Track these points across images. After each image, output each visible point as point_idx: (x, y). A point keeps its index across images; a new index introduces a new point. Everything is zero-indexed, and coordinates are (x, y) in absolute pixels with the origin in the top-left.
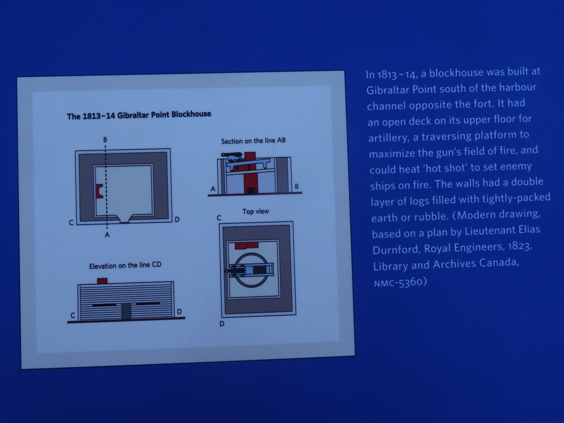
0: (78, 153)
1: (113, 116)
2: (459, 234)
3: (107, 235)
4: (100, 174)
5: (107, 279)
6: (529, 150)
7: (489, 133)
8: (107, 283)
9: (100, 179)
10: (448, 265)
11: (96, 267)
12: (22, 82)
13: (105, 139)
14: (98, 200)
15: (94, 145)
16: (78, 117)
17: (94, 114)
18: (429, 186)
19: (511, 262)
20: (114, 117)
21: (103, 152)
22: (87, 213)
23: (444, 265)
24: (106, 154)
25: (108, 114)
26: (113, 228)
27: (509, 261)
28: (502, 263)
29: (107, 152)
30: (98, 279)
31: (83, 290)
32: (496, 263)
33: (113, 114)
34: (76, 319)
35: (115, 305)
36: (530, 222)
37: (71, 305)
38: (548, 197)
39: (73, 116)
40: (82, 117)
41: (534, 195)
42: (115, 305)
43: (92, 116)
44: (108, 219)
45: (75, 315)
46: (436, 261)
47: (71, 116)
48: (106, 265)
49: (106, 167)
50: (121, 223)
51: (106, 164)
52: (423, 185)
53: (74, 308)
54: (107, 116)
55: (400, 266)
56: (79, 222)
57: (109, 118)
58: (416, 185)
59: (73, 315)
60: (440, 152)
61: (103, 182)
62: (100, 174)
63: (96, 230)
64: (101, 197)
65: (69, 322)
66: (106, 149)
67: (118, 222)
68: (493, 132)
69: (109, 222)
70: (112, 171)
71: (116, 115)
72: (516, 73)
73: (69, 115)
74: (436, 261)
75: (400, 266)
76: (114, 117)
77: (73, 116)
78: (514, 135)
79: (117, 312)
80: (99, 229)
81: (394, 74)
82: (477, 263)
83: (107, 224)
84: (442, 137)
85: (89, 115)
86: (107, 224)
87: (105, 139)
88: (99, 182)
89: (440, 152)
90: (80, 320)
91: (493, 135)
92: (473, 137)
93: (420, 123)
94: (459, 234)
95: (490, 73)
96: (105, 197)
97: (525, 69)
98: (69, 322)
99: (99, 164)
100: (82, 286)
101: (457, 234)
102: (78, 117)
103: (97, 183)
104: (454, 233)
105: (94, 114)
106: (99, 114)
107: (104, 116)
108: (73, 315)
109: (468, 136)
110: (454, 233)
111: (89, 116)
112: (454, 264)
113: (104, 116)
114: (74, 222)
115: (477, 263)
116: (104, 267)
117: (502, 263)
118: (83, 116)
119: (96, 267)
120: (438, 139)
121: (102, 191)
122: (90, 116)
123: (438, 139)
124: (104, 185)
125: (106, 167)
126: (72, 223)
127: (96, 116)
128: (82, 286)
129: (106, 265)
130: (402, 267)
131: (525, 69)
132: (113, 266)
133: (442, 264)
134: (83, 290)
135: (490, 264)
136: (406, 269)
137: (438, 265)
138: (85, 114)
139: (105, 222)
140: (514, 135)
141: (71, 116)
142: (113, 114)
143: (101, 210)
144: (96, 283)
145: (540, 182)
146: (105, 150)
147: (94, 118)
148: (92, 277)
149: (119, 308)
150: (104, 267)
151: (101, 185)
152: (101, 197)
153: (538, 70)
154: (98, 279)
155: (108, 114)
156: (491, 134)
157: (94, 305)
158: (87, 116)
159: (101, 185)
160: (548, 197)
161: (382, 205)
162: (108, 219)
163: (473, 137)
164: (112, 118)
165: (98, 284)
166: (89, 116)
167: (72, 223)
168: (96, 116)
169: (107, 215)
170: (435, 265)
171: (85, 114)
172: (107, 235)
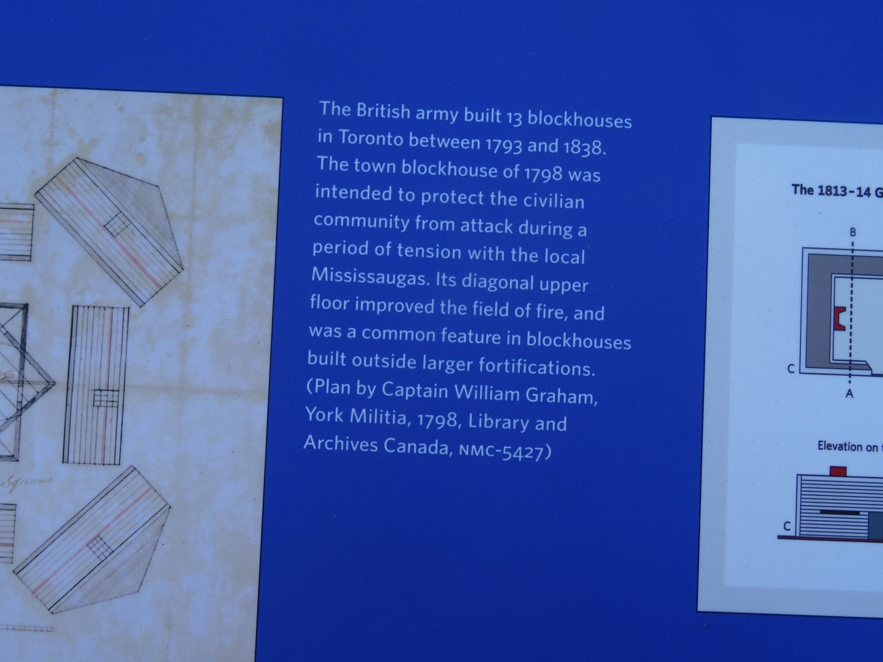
0: (806, 252)
1: (868, 193)
2: (371, 393)
3: (849, 393)
4: (841, 290)
5: (845, 469)
7: (470, 221)
8: (845, 476)
9: (841, 300)
10: (330, 445)
11: (829, 447)
12: (719, 125)
13: (853, 232)
14: (836, 332)
15: (835, 240)
16: (810, 191)
17: (836, 188)
18: (564, 316)
19: (439, 448)
20: (869, 195)
21: (849, 253)
22: (818, 356)
23: (323, 444)
24: (852, 257)
25: (860, 189)
26: (860, 383)
27: (436, 445)
28: (424, 449)
29: (856, 253)
30: (831, 468)
31: (805, 484)
32: (412, 447)
33: (868, 189)
34: (792, 533)
35: (857, 513)
36: (572, 384)
37: (784, 508)
39: (802, 188)
40: (817, 191)
41: (562, 337)
42: (857, 513)
43: (833, 191)
44: (852, 366)
45: (791, 526)
46: (310, 436)
47: (799, 188)
48: (845, 445)
49: (852, 278)
50: (873, 375)
51: (852, 273)
52: (553, 313)
53: (788, 511)
54: (857, 192)
55: (515, 422)
56: (804, 369)
57: (860, 195)
58: (542, 312)
59: (787, 526)
61: (847, 304)
62: (841, 290)
63: (833, 384)
64: (843, 328)
65: (780, 537)
66: (854, 248)
67: (869, 373)
68: (477, 221)
69: (853, 372)
70: (862, 285)
71: (872, 192)
72: (480, 118)
73: (795, 186)
74: (310, 436)
76: (869, 195)
77: (802, 188)
78: (450, 225)
79: (861, 525)
80: (837, 383)
81: (518, 117)
82: (380, 446)
83: (850, 375)
85: (829, 188)
86: (850, 375)
87: (853, 232)
88: (839, 303)
90: (798, 535)
91: (477, 226)
93: (467, 200)
94: (371, 393)
95: (422, 114)
96: (848, 328)
97: (495, 111)
98: (780, 537)
99: (842, 274)
100: (804, 478)
101: (368, 393)
102: (810, 191)
103: (837, 305)
104: (361, 390)
105: (836, 188)
106: (845, 188)
107: (853, 192)
108: (787, 526)
109: (568, 229)
110: (361, 390)
111: (828, 191)
112: (339, 444)
113: (853, 192)
114: (795, 369)
115: (380, 446)
116: (841, 447)
117: (424, 449)
118: (819, 191)
119: (829, 447)
121: (844, 319)
122: (830, 190)
124: (848, 309)
125: (852, 278)
126: (792, 369)
127: (840, 191)
128: (804, 478)
129: (845, 445)
131: (495, 111)
132: (857, 448)
133: (320, 442)
134: (805, 484)
135: (402, 448)
137: (313, 443)
138: (821, 187)
139: (847, 372)
140: (450, 225)
141: (799, 188)
142: (868, 189)
143: (840, 352)
144: (828, 473)
146: (853, 250)
147: (836, 194)
148: (821, 464)
149: (863, 519)
150: (841, 447)
151: (843, 309)
152: (843, 328)
154: (831, 468)
155: (860, 189)
156: (473, 223)
157: (823, 512)
158: (824, 191)
159: (843, 309)
162: (852, 366)
164: (865, 197)
165: (831, 475)
166: (828, 191)
167: (792, 369)
168: (840, 191)
169: (850, 361)
170: (307, 443)
171: (821, 187)
172: (849, 393)
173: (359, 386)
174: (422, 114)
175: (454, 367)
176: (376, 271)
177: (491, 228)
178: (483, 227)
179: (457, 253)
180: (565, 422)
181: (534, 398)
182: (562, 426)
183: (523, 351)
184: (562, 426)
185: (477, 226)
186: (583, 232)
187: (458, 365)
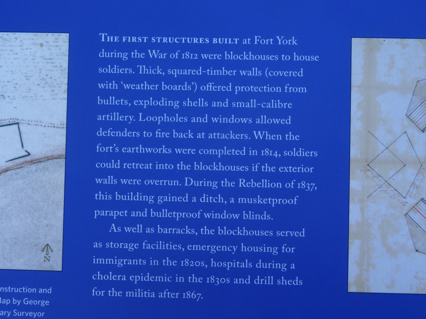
2: (19, 303)
6: (45, 291)
38: (303, 90)
55: (5, 312)
60: (44, 301)
75: (5, 312)
84: (30, 314)
89: (44, 301)
91: (216, 136)
92: (155, 199)
95: (41, 291)
101: (17, 303)
104: (15, 302)
110: (15, 302)
120: (27, 315)
123: (27, 315)
130: (7, 313)
136: (9, 315)
145: (296, 138)
153: (203, 134)
160: (303, 90)
161: (35, 316)
163: (155, 199)
173: (14, 300)
174: (41, 291)
175: (45, 303)
176: (198, 45)
177: (224, 136)
178: (220, 136)
179: (34, 290)
180: (51, 289)
181: (27, 303)
182: (49, 291)
183: (241, 223)
184: (49, 291)
185: (216, 136)
186: (293, 267)
187: (46, 303)
